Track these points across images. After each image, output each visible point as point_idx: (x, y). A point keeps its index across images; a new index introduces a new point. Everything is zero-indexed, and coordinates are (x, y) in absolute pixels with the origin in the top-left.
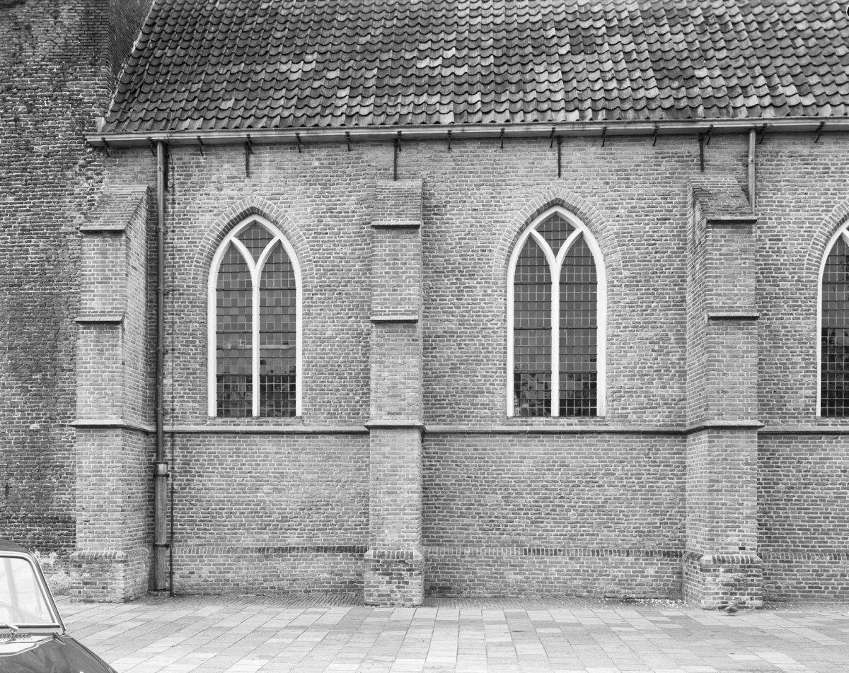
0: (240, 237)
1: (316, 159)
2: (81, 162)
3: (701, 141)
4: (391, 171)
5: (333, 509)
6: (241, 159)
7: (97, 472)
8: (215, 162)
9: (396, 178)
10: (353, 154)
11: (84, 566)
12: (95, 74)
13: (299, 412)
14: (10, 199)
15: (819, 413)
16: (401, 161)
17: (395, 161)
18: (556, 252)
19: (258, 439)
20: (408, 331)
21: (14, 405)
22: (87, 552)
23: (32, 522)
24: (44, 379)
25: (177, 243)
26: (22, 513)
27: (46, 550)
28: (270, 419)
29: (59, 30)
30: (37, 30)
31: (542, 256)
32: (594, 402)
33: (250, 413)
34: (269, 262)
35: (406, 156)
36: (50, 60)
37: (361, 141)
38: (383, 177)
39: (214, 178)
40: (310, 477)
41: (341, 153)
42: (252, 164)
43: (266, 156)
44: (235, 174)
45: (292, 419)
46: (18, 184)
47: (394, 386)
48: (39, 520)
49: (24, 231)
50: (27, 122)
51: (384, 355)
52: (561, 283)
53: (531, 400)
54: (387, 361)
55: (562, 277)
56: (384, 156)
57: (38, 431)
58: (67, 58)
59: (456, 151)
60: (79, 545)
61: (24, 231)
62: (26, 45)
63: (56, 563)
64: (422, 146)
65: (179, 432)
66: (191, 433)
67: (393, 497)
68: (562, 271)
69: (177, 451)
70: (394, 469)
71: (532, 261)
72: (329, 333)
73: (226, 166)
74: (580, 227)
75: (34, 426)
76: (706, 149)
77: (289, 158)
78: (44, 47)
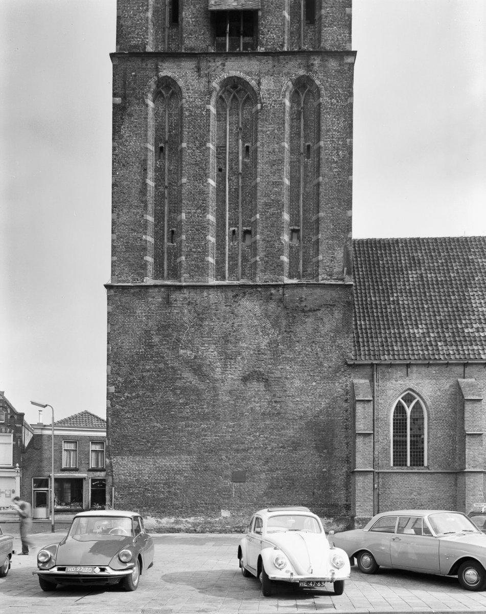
0: (402, 398)
1: (433, 370)
2: (343, 370)
3: (464, 366)
4: (463, 375)
5: (440, 501)
6: (405, 370)
7: (363, 488)
8: (395, 371)
9: (464, 378)
10: (448, 369)
11: (360, 522)
12: (348, 337)
13: (426, 464)
14: (314, 384)
15: (392, 465)
16: (466, 372)
17: (464, 371)
18: (408, 407)
19: (411, 475)
20: (9, 437)
21: (317, 462)
22: (360, 517)
23: (323, 506)
24: (328, 452)
25: (380, 401)
26: (319, 503)
27: (329, 517)
28: (414, 467)
29: (334, 320)
30: (325, 320)
31: (403, 407)
32: (423, 461)
33: (406, 465)
34: (414, 407)
35: (468, 370)
36: (331, 331)
37: (452, 364)
38: (460, 377)
39: (394, 377)
40: (431, 489)
41: (443, 368)
42: (409, 372)
43: (415, 369)
44: (403, 375)
45: (423, 467)
46: (318, 378)
47: (474, 457)
48: (326, 505)
49: (320, 396)
50: (321, 354)
51: (470, 446)
52: (423, 418)
53: (399, 460)
54: (472, 448)
55: (411, 416)
56: (460, 370)
57: (325, 471)
58: (337, 331)
59: (430, 369)
60: (357, 514)
61: (320, 396)
62: (321, 326)
63: (333, 522)
64: (474, 366)
65: (381, 472)
66: (385, 472)
67: (474, 497)
68: (411, 413)
69: (380, 479)
70: (475, 487)
71: (400, 409)
72: (439, 435)
73: (399, 372)
74: (418, 398)
75: (325, 470)
76: (466, 369)
77: (424, 370)
78: (328, 326)
